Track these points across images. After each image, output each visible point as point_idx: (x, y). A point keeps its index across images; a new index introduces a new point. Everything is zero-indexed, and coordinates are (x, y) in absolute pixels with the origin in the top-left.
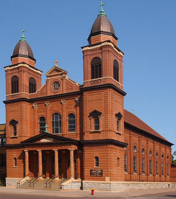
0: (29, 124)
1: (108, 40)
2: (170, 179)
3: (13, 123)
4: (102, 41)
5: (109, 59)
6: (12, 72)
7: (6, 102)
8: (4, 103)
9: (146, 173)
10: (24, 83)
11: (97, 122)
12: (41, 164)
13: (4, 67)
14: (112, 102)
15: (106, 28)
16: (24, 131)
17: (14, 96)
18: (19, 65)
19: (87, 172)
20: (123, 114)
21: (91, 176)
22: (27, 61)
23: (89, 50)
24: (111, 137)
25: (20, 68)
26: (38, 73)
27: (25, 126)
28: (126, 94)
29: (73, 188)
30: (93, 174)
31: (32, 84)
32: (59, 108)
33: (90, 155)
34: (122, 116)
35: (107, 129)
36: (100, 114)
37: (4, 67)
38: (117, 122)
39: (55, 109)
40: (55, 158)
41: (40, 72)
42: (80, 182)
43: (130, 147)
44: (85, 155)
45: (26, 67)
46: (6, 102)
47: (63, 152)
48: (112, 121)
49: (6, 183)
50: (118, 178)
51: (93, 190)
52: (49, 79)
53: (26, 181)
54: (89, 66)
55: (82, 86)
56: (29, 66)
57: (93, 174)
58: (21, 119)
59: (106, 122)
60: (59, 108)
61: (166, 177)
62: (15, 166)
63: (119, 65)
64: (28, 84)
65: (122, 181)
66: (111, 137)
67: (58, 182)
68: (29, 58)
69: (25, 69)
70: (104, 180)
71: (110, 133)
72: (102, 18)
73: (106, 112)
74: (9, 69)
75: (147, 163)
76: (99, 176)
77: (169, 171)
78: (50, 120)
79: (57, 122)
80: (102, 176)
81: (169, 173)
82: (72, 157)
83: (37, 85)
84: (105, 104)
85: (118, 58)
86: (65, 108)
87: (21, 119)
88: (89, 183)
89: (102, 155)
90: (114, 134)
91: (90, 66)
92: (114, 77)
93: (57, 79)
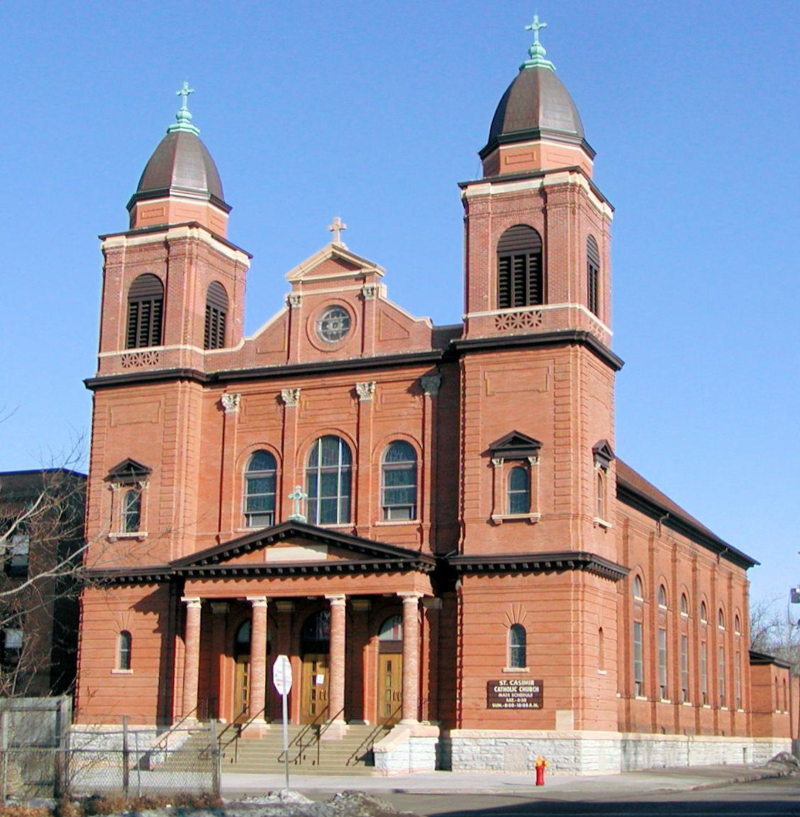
2: (748, 724)
3: (130, 472)
7: (95, 385)
8: (88, 387)
10: (191, 308)
11: (523, 478)
13: (100, 237)
15: (558, 116)
17: (140, 360)
19: (471, 691)
21: (489, 707)
25: (174, 244)
28: (623, 363)
30: (503, 701)
35: (565, 511)
37: (100, 237)
39: (323, 419)
41: (242, 258)
45: (201, 243)
46: (95, 385)
54: (490, 257)
55: (458, 331)
56: (212, 237)
57: (503, 701)
62: (125, 671)
63: (601, 255)
64: (202, 312)
68: (210, 201)
70: (551, 724)
74: (122, 247)
76: (529, 708)
77: (743, 684)
79: (330, 478)
80: (541, 707)
82: (411, 629)
83: (231, 311)
88: (482, 742)
91: (493, 259)
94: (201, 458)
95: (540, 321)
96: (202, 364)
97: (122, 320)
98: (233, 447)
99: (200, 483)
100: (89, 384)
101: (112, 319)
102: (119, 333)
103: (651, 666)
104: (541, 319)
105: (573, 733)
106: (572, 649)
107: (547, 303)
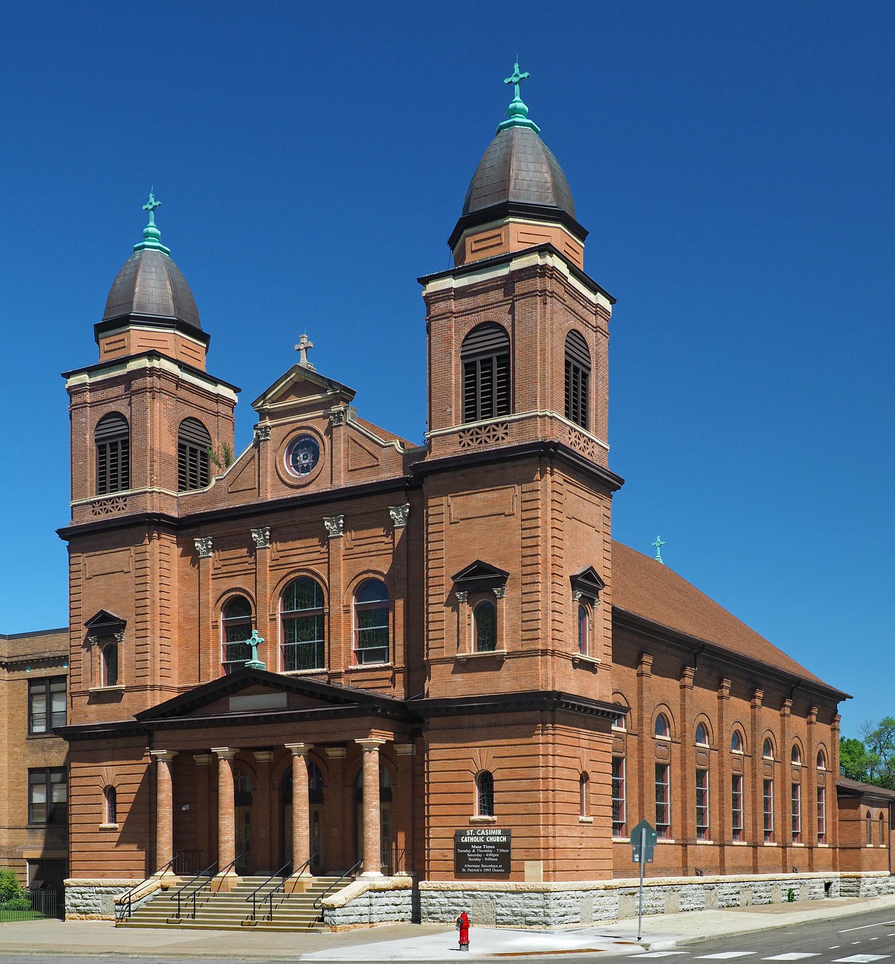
0: (177, 631)
1: (542, 241)
4: (515, 247)
5: (543, 329)
6: (100, 395)
9: (780, 839)
10: (157, 447)
12: (232, 810)
14: (558, 525)
16: (154, 664)
17: (109, 507)
18: (133, 366)
20: (609, 573)
22: (170, 344)
23: (456, 290)
24: (550, 681)
26: (218, 395)
27: (158, 641)
29: (375, 918)
31: (191, 449)
32: (316, 556)
33: (452, 765)
34: (604, 585)
36: (501, 578)
38: (577, 613)
39: (295, 559)
40: (295, 781)
42: (406, 888)
43: (640, 719)
44: (433, 766)
45: (163, 374)
47: (330, 753)
48: (557, 607)
49: (67, 902)
50: (583, 865)
51: (464, 915)
52: (268, 424)
53: (160, 890)
54: (453, 363)
56: (180, 367)
58: (141, 610)
59: (527, 617)
60: (316, 556)
61: (755, 847)
62: (112, 825)
65: (601, 877)
66: (550, 681)
67: (308, 890)
69: (158, 383)
71: (545, 663)
72: (516, 142)
73: (528, 570)
75: (721, 790)
77: (830, 820)
78: (275, 609)
81: (827, 830)
82: (370, 777)
84: (527, 533)
85: (587, 323)
86: (342, 552)
87: (140, 611)
88: (450, 894)
89: (507, 763)
90: (565, 666)
91: (457, 384)
92: (567, 408)
93: (305, 424)
94: (179, 606)
95: (506, 434)
96: (176, 507)
97: (91, 464)
98: (208, 594)
99: (179, 633)
100: (63, 533)
101: (80, 463)
102: (88, 479)
103: (682, 807)
104: (507, 431)
105: (541, 885)
106: (541, 796)
107: (514, 412)
